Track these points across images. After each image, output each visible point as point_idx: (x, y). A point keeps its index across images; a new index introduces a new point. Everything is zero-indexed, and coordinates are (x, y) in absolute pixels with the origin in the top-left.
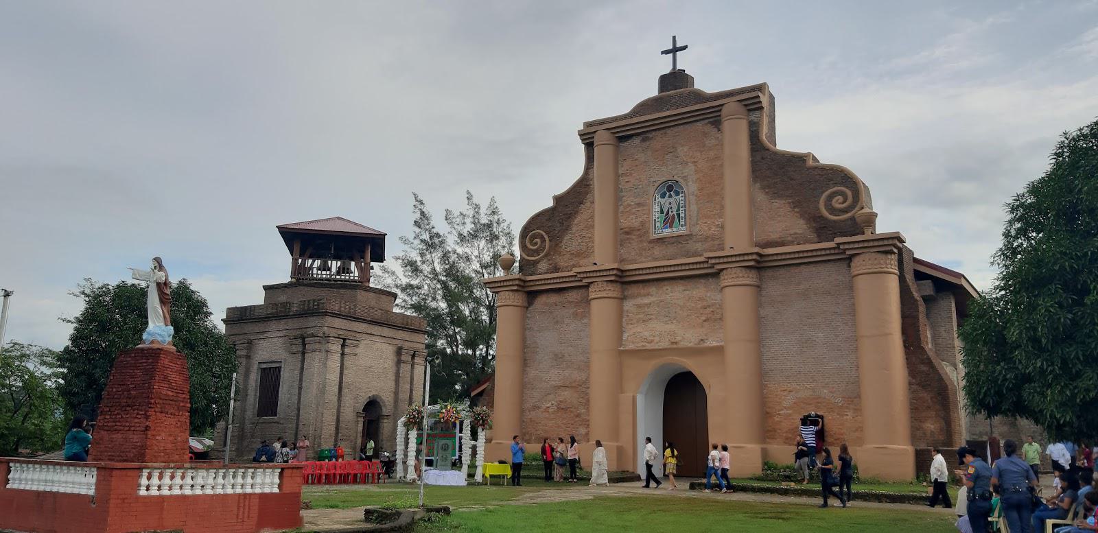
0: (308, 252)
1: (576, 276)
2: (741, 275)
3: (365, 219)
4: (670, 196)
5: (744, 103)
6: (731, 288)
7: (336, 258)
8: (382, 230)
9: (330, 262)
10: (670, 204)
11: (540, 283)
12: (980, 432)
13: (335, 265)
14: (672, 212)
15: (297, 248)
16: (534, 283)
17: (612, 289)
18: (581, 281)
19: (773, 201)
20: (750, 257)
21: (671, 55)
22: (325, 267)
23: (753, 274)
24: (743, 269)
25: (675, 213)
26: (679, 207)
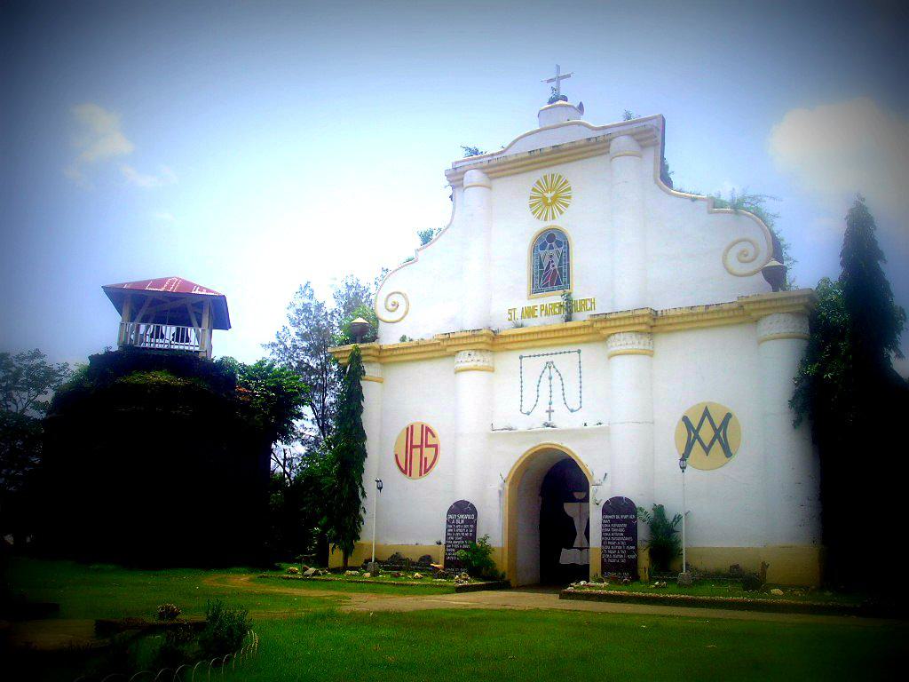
0: (139, 317)
1: (439, 344)
2: (476, 359)
3: (204, 278)
4: (551, 248)
5: (636, 137)
6: (626, 357)
7: (171, 323)
8: (219, 290)
9: (164, 327)
10: (551, 256)
11: (409, 351)
12: (553, 484)
13: (169, 331)
14: (553, 266)
15: (126, 310)
16: (401, 352)
17: (482, 359)
18: (445, 350)
19: (197, 349)
20: (641, 320)
21: (562, 74)
22: (158, 334)
23: (645, 339)
24: (633, 335)
25: (556, 267)
26: (561, 261)
